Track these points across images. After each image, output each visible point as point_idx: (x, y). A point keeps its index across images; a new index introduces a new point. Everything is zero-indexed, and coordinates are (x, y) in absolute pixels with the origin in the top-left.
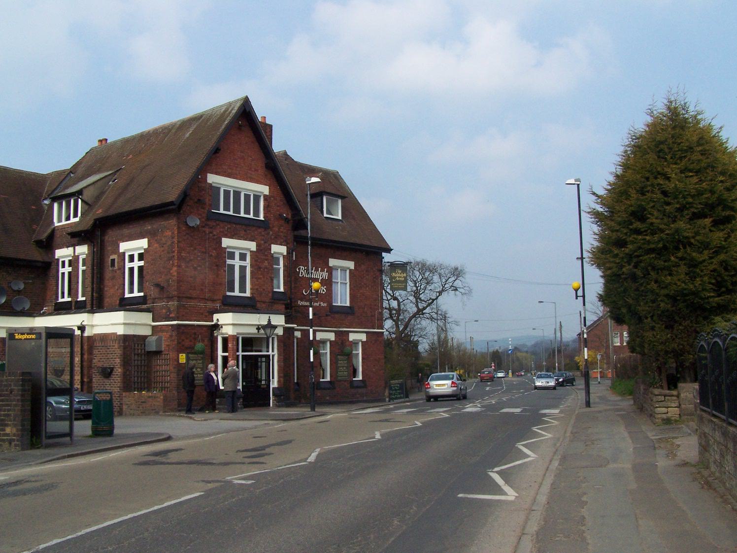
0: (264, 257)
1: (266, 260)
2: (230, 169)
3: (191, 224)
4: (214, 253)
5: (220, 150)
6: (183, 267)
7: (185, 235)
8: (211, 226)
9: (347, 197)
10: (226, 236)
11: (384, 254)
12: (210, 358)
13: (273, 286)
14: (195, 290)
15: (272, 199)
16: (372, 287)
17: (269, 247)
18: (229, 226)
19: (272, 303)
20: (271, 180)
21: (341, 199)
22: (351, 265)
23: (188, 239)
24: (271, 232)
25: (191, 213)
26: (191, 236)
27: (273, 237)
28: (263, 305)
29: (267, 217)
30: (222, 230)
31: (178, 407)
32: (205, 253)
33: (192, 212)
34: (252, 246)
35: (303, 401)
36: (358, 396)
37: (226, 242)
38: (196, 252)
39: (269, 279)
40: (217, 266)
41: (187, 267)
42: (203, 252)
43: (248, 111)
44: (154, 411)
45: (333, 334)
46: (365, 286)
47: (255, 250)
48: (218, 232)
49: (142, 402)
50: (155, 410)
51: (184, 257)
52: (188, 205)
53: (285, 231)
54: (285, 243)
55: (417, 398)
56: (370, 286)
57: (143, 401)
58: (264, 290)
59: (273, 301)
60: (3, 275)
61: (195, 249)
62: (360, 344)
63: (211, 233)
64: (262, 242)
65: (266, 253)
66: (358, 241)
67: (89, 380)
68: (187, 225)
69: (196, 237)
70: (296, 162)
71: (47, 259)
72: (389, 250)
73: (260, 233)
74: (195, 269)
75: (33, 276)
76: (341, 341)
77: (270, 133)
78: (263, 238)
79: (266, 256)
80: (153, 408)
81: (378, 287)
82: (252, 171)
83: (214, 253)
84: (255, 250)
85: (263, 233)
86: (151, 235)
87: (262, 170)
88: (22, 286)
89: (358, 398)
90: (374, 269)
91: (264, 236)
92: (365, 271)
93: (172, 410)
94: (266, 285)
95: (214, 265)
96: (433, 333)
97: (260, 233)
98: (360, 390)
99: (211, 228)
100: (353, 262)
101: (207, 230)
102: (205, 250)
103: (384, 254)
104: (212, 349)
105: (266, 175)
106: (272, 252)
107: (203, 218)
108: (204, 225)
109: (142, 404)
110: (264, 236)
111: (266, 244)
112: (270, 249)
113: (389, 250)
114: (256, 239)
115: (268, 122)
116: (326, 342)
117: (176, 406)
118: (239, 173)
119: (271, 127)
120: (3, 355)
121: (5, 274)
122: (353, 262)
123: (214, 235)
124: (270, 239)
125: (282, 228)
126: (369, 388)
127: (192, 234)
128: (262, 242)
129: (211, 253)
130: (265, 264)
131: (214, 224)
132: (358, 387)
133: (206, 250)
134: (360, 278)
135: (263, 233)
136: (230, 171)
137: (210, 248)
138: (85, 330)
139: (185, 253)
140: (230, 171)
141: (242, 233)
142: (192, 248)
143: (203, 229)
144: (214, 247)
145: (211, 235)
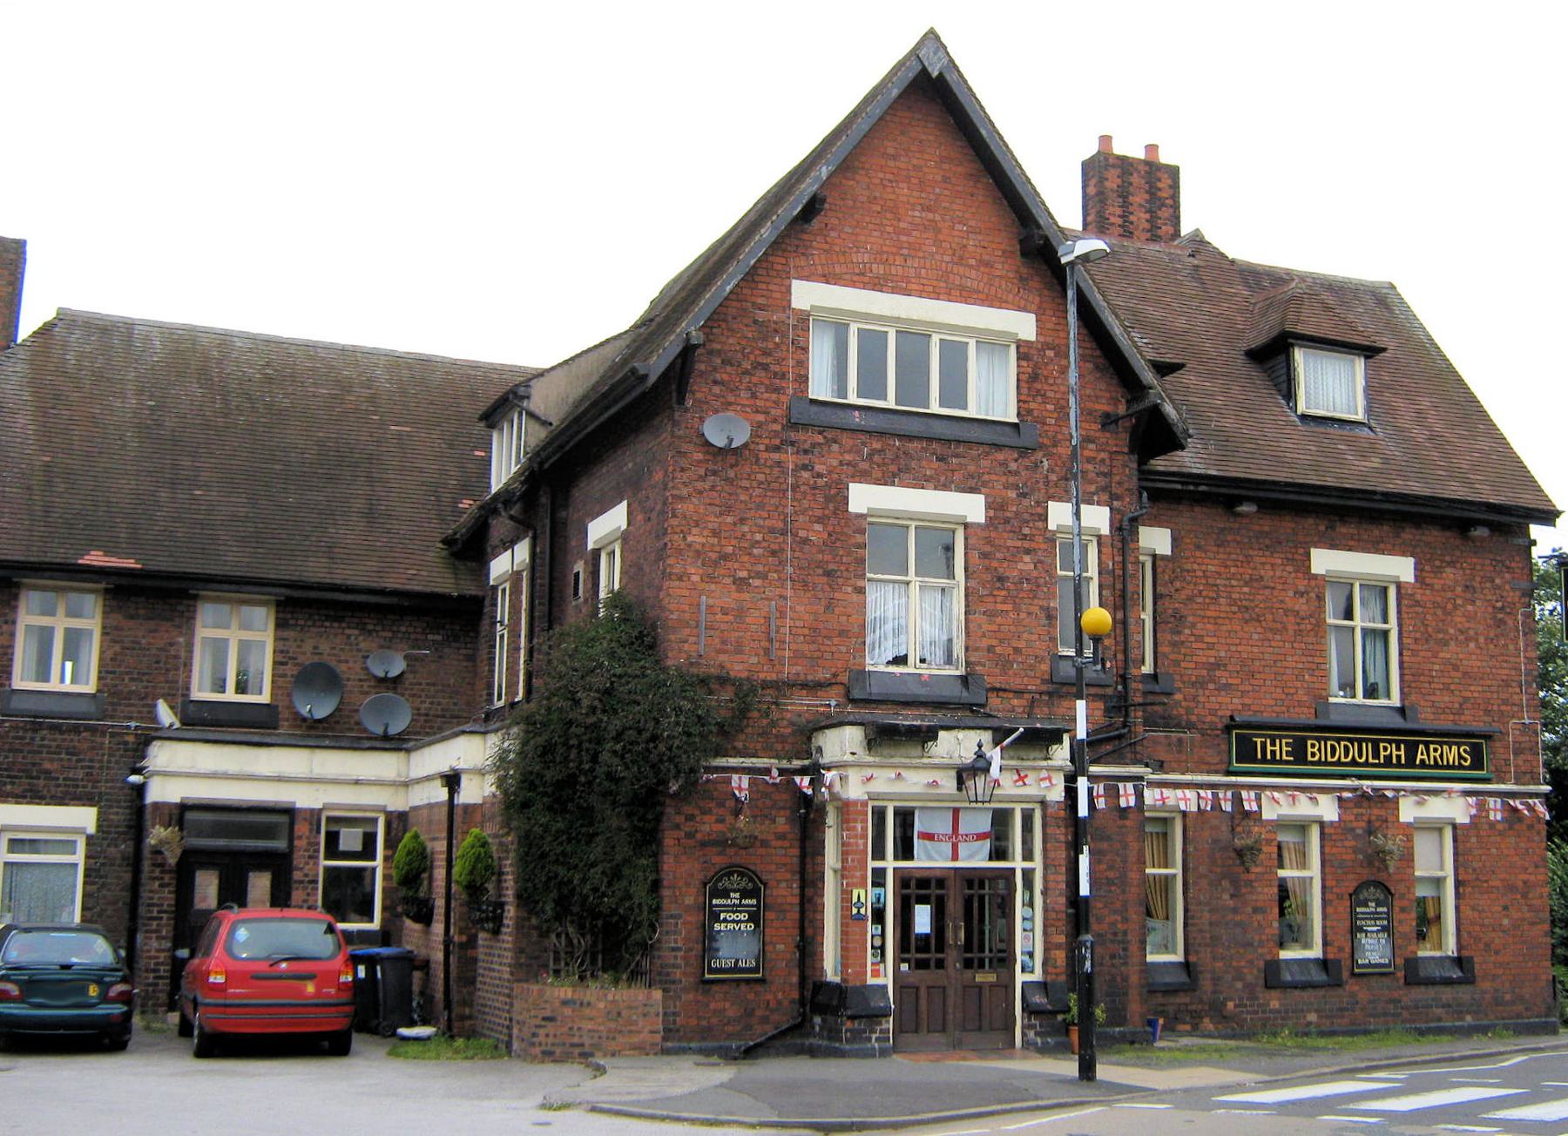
0: (1019, 544)
1: (1028, 552)
2: (881, 262)
3: (719, 441)
4: (816, 533)
5: (823, 201)
6: (696, 578)
7: (703, 478)
8: (807, 446)
9: (1384, 350)
10: (864, 477)
11: (1536, 531)
12: (797, 877)
13: (1053, 639)
14: (741, 652)
15: (1050, 353)
16: (1489, 640)
17: (1039, 510)
18: (877, 445)
19: (1050, 694)
20: (1046, 292)
21: (1367, 357)
22: (1401, 568)
23: (713, 488)
24: (1046, 463)
25: (727, 405)
26: (727, 479)
27: (1053, 477)
28: (1015, 702)
29: (1030, 412)
30: (848, 457)
31: (664, 1039)
32: (784, 533)
33: (730, 404)
34: (972, 507)
35: (1207, 1024)
36: (1439, 1011)
37: (863, 497)
38: (746, 528)
39: (1042, 615)
40: (828, 574)
41: (710, 579)
42: (772, 530)
43: (935, 74)
44: (577, 1051)
45: (1460, 802)
46: (1461, 638)
47: (982, 519)
48: (835, 463)
49: (544, 1019)
50: (582, 1045)
51: (699, 547)
52: (715, 382)
53: (1103, 455)
54: (1105, 497)
55: (1542, 1046)
56: (1482, 639)
57: (548, 1013)
58: (1017, 650)
59: (1051, 687)
60: (349, 637)
61: (742, 521)
62: (1315, 835)
63: (805, 467)
64: (1012, 494)
65: (1026, 531)
66: (1416, 488)
67: (464, 938)
68: (708, 444)
69: (746, 483)
70: (1233, 262)
71: (471, 589)
72: (1548, 516)
73: (1004, 464)
74: (741, 583)
75: (439, 638)
76: (1363, 824)
77: (1171, 192)
78: (1011, 479)
79: (1030, 537)
80: (576, 1040)
81: (1515, 640)
82: (971, 267)
83: (816, 533)
84: (982, 519)
85: (1013, 466)
86: (630, 488)
87: (1007, 266)
88: (397, 667)
89: (1440, 1019)
90: (1498, 581)
91: (1016, 473)
92: (1459, 589)
93: (641, 1049)
94: (1025, 635)
95: (820, 571)
96: (665, 722)
97: (1004, 464)
98: (1447, 994)
99: (806, 452)
100: (1411, 560)
101: (790, 458)
102: (781, 525)
103: (1536, 531)
104: (803, 849)
105: (1021, 279)
106: (1052, 526)
107: (775, 421)
108: (777, 442)
109: (543, 1023)
110: (1016, 473)
111: (1026, 502)
112: (1044, 518)
113: (1548, 516)
114: (985, 484)
115: (1165, 158)
116: (1309, 826)
117: (658, 1038)
118: (919, 276)
119: (1174, 172)
120: (310, 857)
121: (356, 632)
122: (1411, 560)
123: (820, 475)
124: (1041, 485)
125: (1092, 446)
126: (1486, 985)
127: (731, 474)
128: (1012, 494)
129: (802, 534)
130: (1020, 566)
131: (820, 439)
132: (1431, 982)
133: (785, 523)
134: (1439, 612)
135: (1013, 466)
136: (879, 269)
137: (801, 518)
138: (458, 784)
139: (701, 535)
140: (879, 269)
141: (931, 467)
142: (729, 519)
143: (776, 456)
144: (818, 513)
145: (806, 475)
